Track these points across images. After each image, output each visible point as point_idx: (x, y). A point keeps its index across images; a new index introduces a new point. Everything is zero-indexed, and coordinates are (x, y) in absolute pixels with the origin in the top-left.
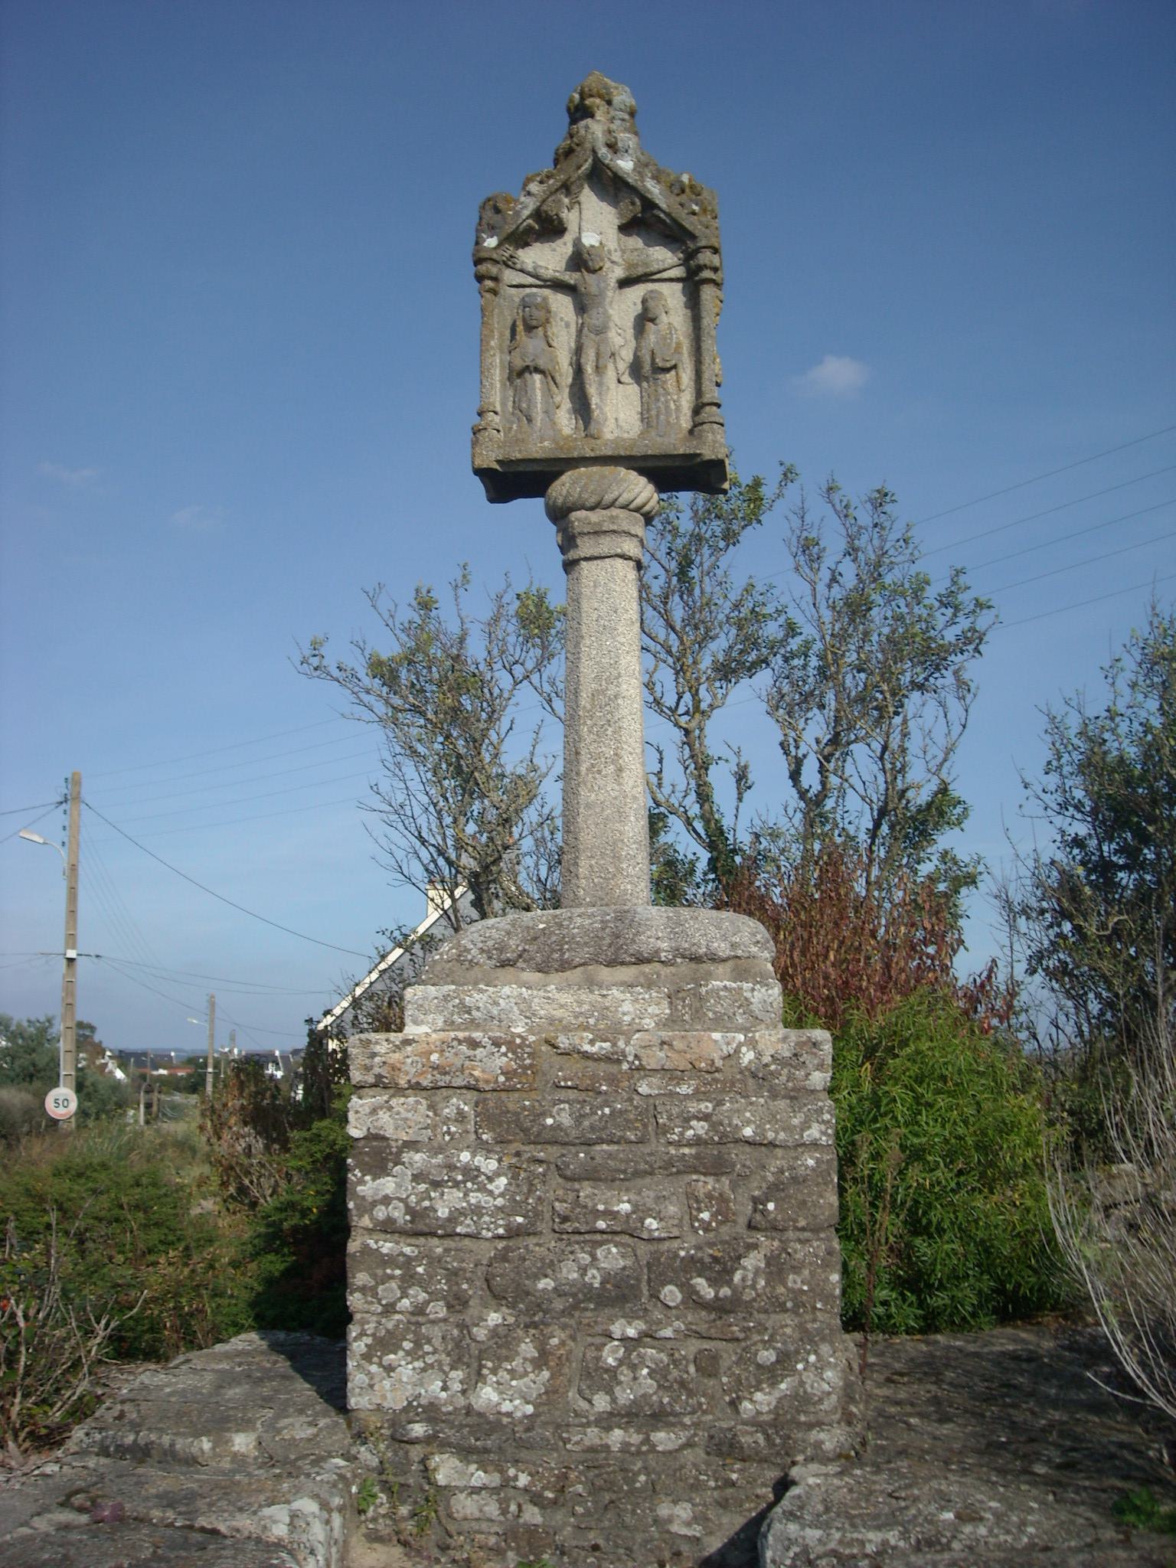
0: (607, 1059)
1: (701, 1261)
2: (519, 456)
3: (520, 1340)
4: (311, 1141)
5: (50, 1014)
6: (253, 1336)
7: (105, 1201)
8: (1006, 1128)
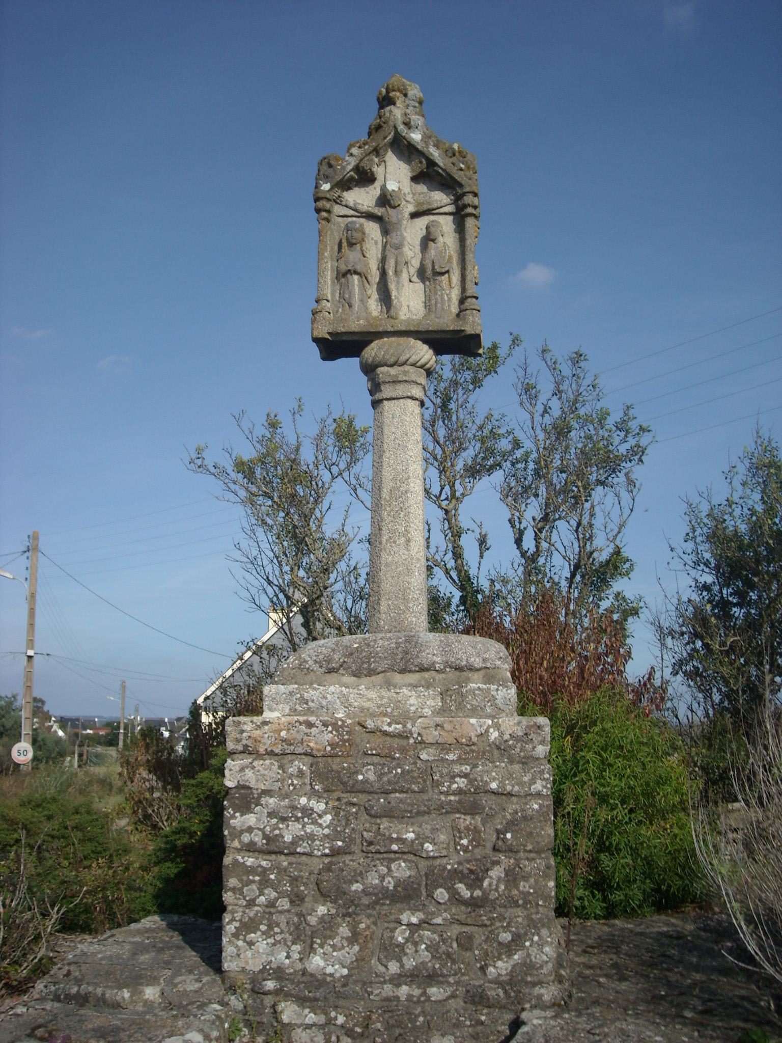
0: (400, 736)
1: (461, 872)
2: (343, 330)
3: (339, 925)
4: (197, 786)
5: (15, 692)
6: (157, 918)
7: (55, 824)
8: (661, 781)
